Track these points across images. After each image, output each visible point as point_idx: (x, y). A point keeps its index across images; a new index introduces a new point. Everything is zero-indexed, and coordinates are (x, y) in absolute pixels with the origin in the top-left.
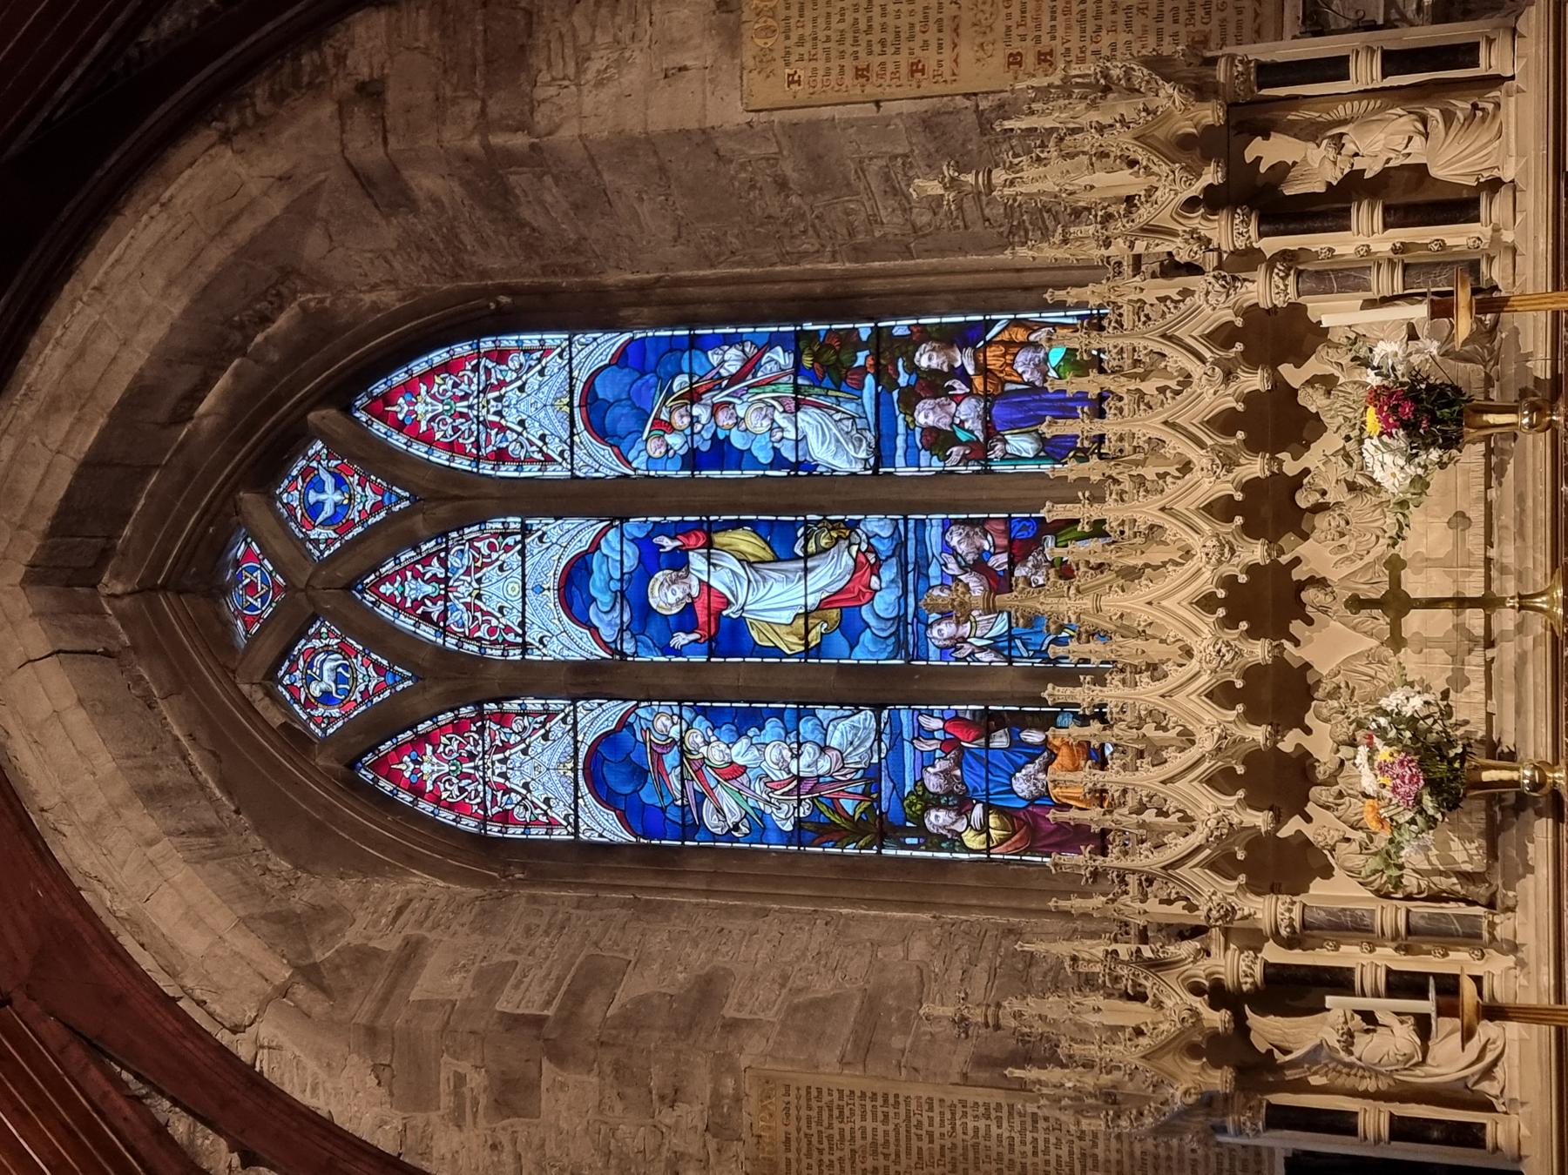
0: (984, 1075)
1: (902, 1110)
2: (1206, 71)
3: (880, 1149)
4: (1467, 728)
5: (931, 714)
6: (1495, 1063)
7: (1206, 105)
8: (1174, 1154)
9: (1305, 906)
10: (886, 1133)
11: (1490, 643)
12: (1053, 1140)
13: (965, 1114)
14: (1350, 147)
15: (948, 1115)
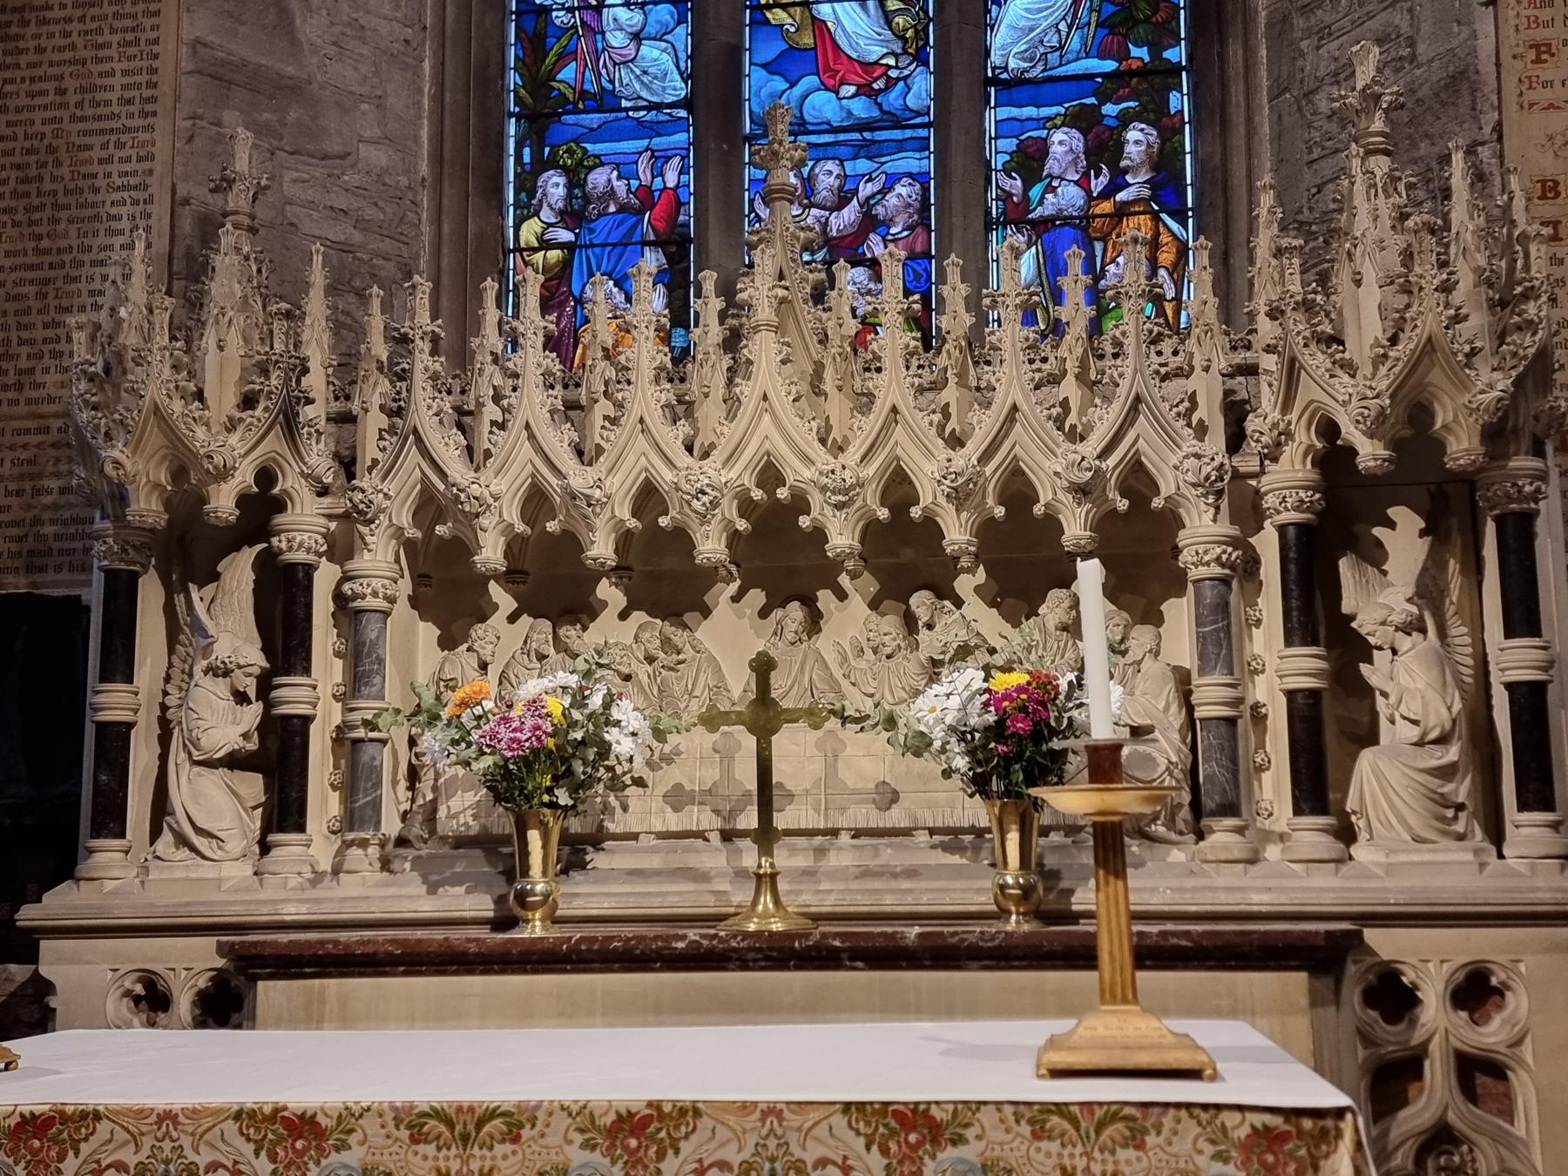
0: (186, 225)
1: (137, 122)
2: (1525, 444)
3: (88, 97)
4: (618, 810)
5: (683, 171)
6: (193, 849)
7: (1476, 440)
9: (387, 614)
10: (108, 103)
11: (728, 836)
13: (135, 202)
14: (1404, 642)
15: (133, 181)
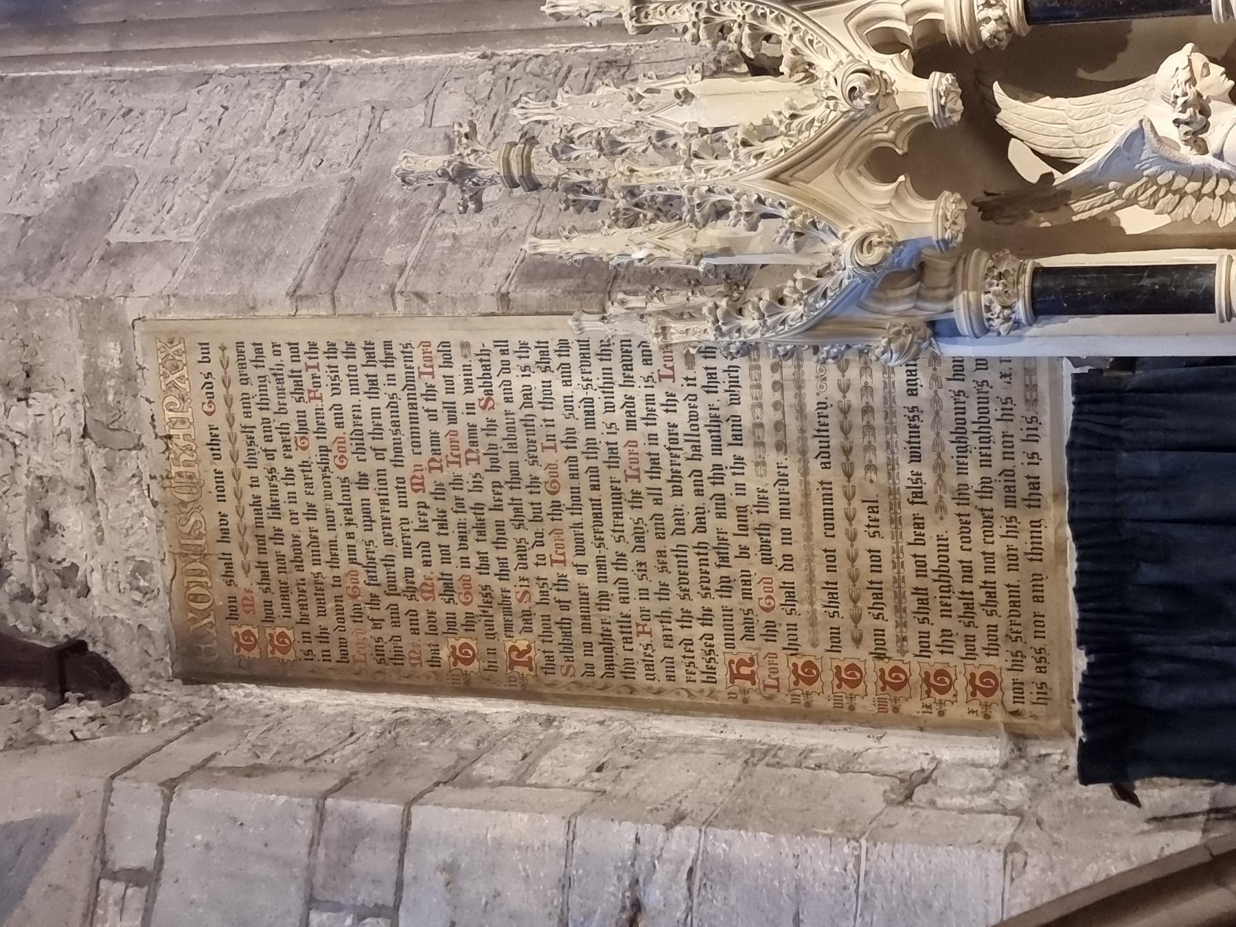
0: (538, 294)
1: (399, 369)
3: (368, 442)
8: (877, 402)
10: (376, 413)
12: (661, 398)
13: (506, 367)
15: (477, 371)
